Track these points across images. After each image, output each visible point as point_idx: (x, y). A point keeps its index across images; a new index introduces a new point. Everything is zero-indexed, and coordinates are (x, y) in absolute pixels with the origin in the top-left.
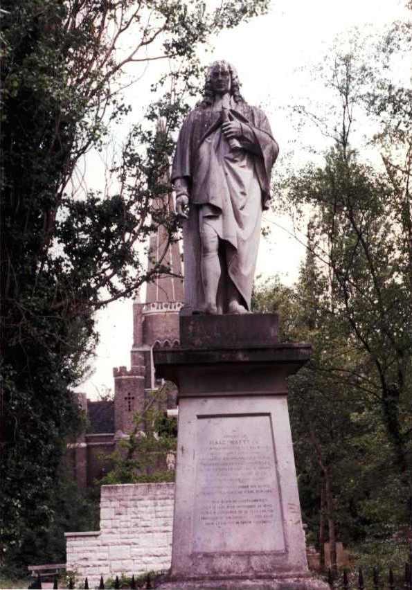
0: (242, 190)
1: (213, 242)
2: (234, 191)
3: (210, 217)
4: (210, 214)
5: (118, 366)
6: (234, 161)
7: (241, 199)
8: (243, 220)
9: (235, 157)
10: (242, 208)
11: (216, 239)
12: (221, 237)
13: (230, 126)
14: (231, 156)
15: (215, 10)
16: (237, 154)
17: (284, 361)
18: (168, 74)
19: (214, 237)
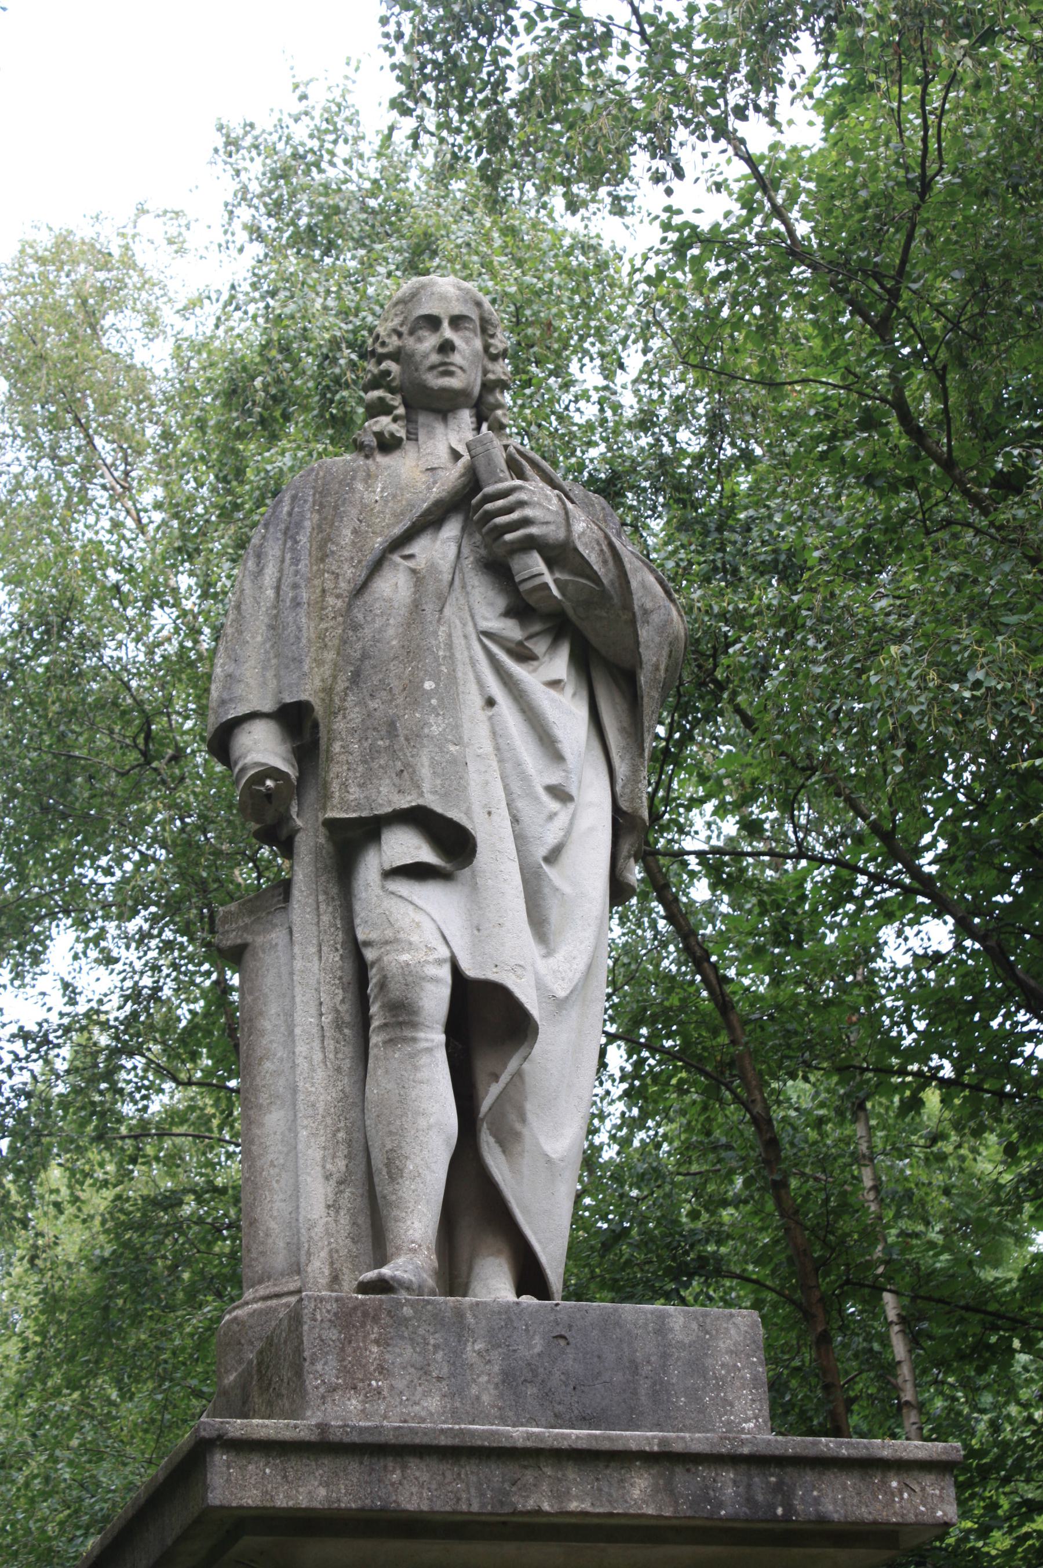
0: (554, 779)
1: (435, 980)
2: (525, 778)
3: (417, 872)
4: (426, 855)
5: (267, 107)
6: (523, 656)
7: (552, 816)
8: (554, 914)
9: (530, 637)
10: (553, 856)
11: (445, 973)
12: (471, 970)
13: (528, 512)
14: (511, 629)
15: (45, 241)
16: (537, 628)
17: (523, 711)
18: (151, 215)
19: (439, 962)
